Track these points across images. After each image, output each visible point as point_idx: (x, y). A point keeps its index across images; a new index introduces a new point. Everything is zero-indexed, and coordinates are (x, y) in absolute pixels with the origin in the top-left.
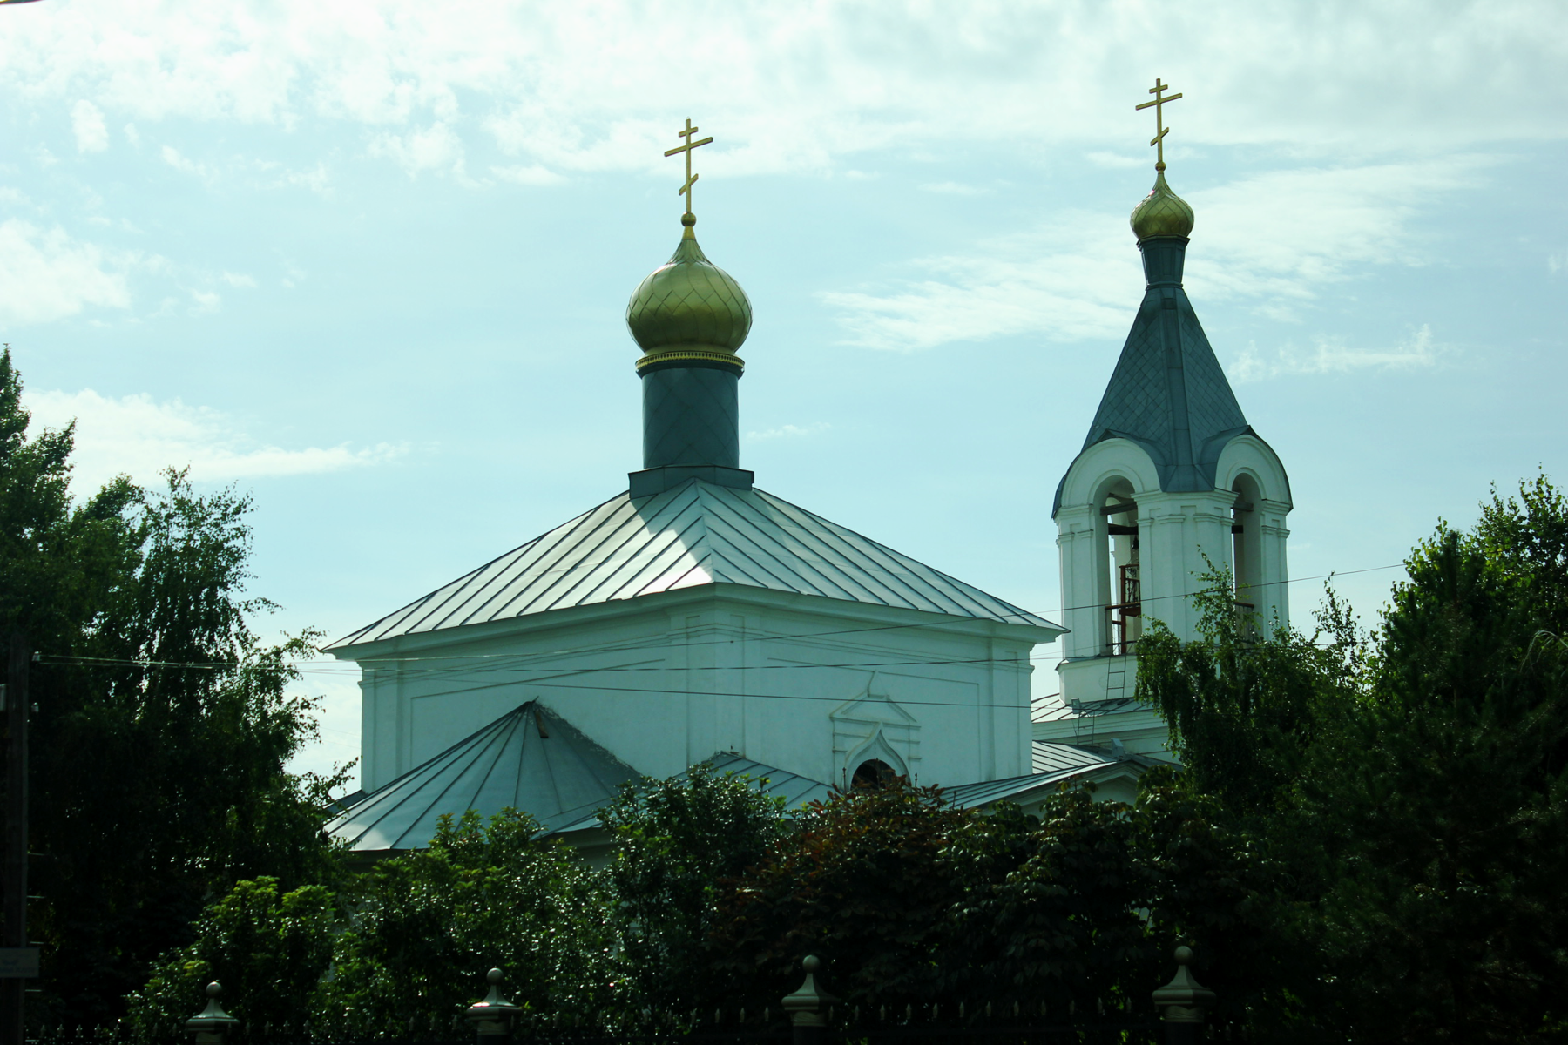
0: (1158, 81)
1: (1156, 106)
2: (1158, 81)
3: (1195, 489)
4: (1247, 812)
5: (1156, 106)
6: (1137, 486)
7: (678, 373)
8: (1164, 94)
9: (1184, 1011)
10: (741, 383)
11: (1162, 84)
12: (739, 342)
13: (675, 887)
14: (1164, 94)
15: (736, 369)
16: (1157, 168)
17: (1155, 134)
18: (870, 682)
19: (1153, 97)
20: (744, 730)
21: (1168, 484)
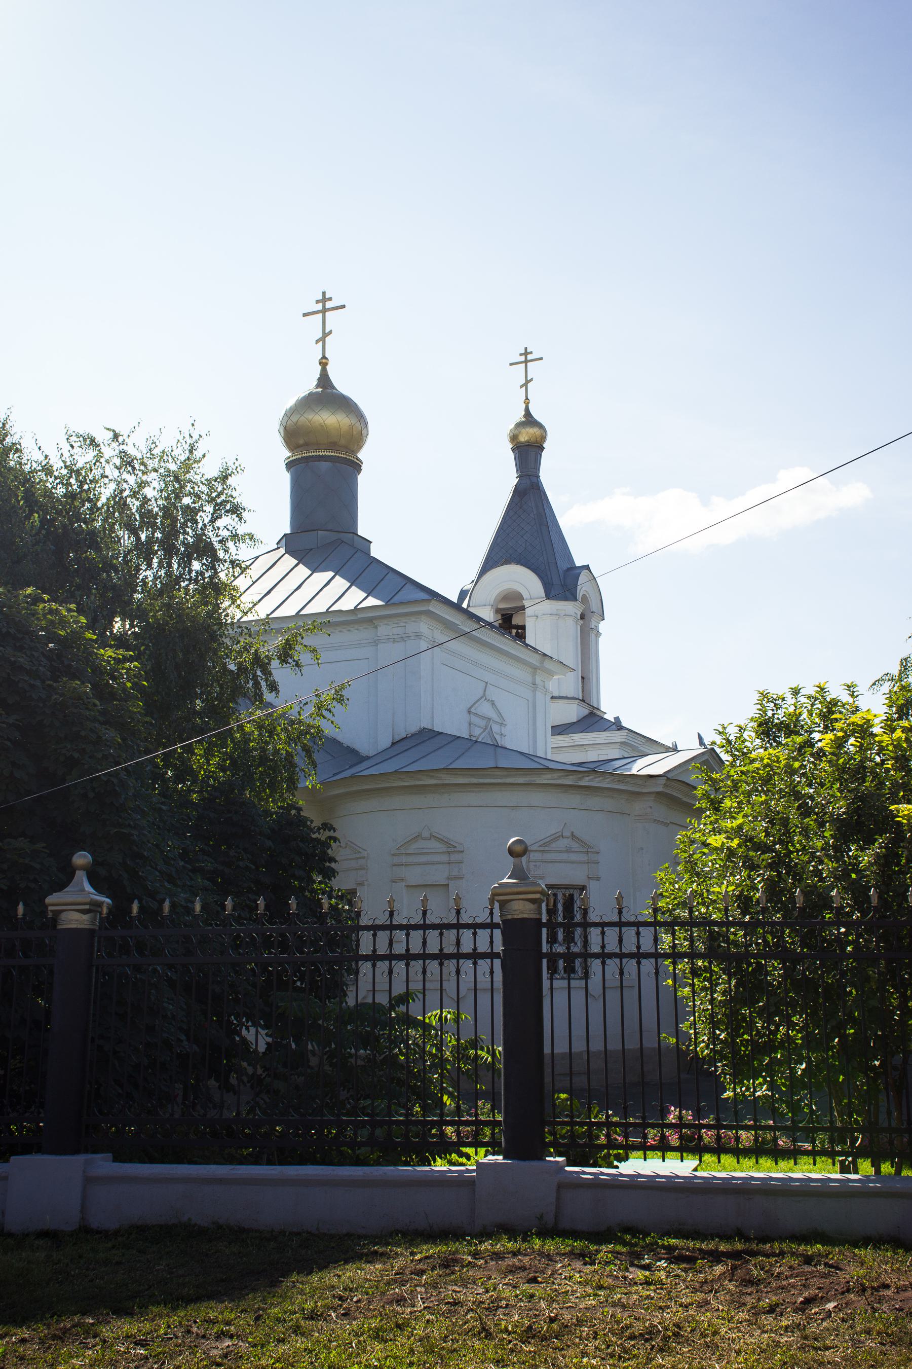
0: (324, 293)
1: (321, 315)
2: (324, 293)
3: (566, 599)
4: (778, 762)
5: (321, 315)
6: (525, 594)
7: (325, 465)
8: (329, 305)
9: (77, 916)
10: (360, 478)
11: (327, 297)
12: (360, 447)
13: (733, 781)
14: (329, 305)
15: (357, 467)
16: (320, 363)
17: (320, 335)
18: (485, 691)
19: (319, 307)
20: (433, 713)
21: (550, 594)
